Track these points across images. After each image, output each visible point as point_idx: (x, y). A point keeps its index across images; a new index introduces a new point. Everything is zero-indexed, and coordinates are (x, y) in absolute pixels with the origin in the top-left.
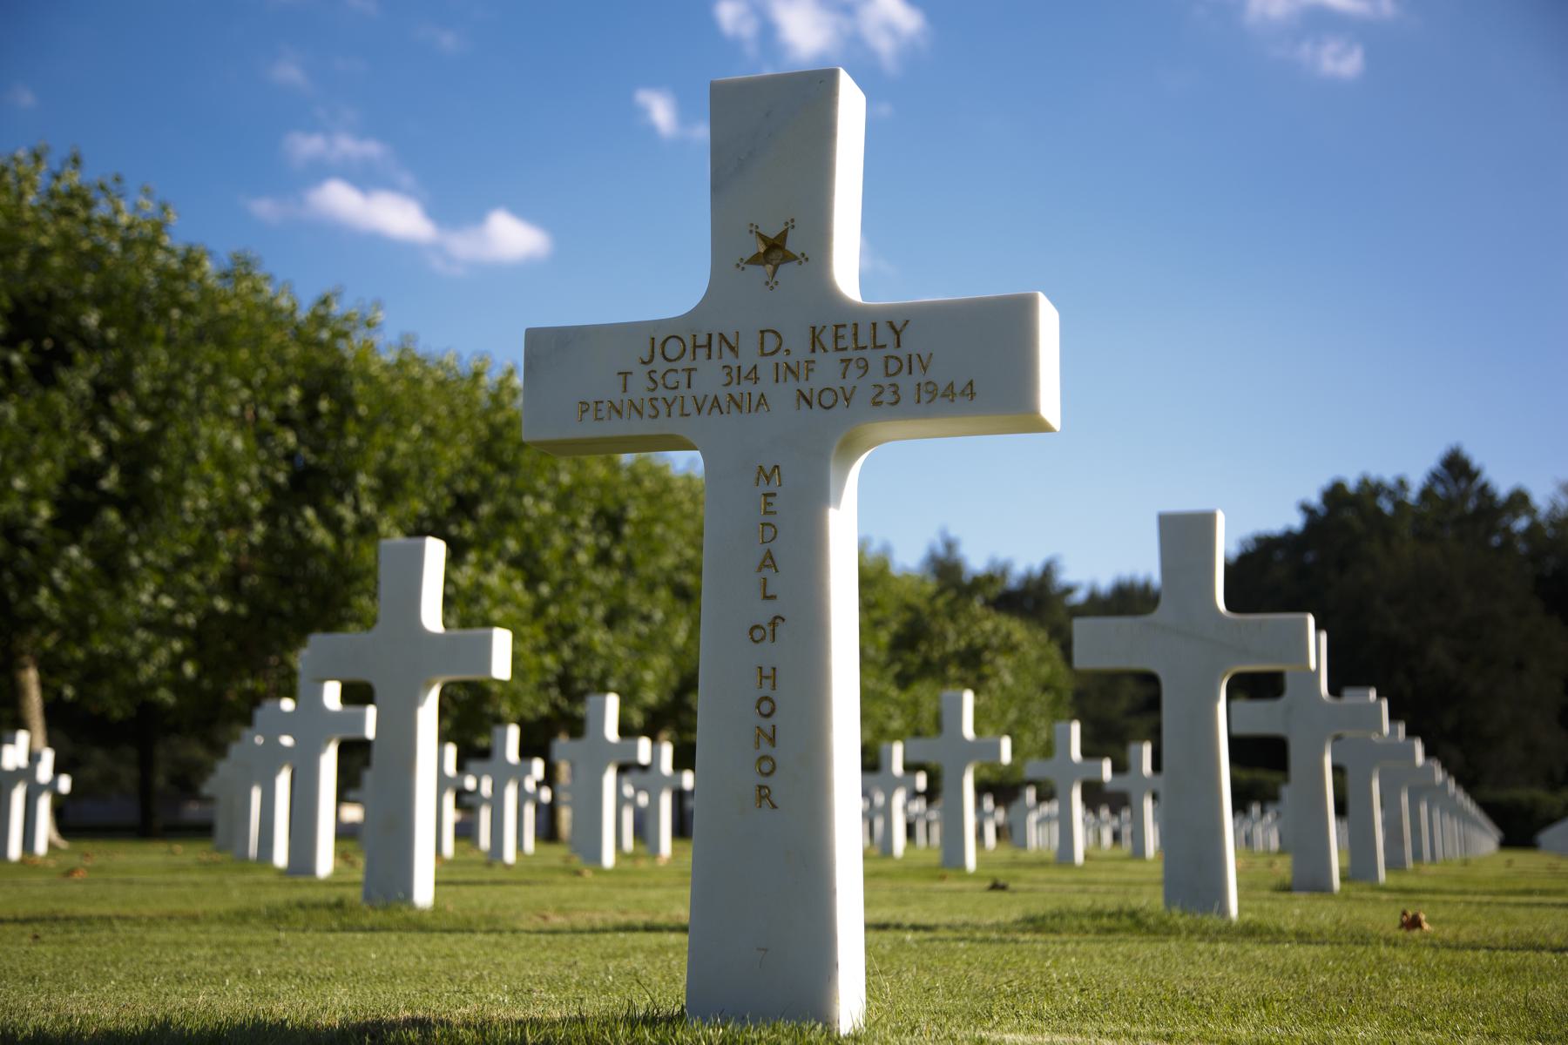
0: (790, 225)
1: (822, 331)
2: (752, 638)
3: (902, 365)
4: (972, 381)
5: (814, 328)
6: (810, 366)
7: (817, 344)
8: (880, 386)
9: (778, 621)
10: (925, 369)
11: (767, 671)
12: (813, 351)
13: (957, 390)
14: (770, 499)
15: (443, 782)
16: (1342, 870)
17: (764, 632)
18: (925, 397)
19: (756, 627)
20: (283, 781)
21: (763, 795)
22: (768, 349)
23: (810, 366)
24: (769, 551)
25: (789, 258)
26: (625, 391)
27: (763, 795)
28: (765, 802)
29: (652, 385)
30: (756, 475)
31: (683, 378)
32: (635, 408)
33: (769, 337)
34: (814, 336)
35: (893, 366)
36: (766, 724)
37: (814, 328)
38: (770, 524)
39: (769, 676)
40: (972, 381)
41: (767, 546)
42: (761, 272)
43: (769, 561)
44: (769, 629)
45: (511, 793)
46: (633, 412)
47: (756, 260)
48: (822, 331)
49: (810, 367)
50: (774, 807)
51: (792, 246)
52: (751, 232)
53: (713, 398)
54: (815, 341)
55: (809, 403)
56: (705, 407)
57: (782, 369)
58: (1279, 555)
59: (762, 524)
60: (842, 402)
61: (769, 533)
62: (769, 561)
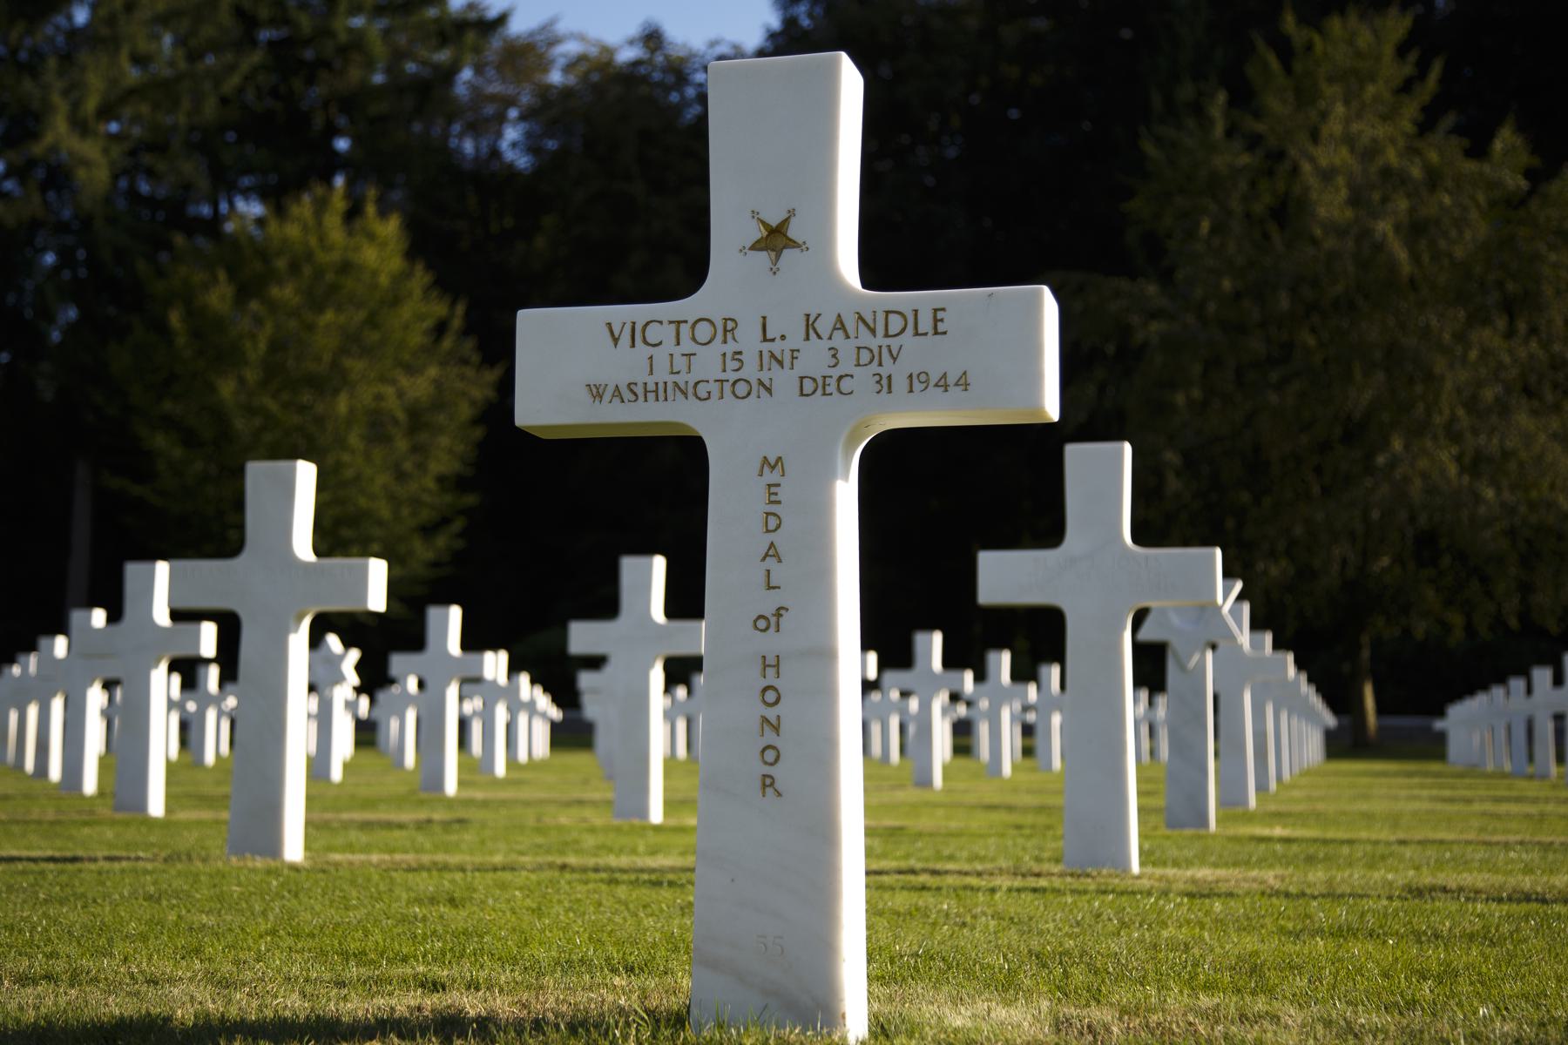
0: (792, 213)
1: (817, 318)
2: (761, 630)
3: (873, 357)
5: (808, 316)
6: (795, 354)
7: (811, 331)
8: (878, 374)
9: (782, 612)
10: (895, 359)
11: (771, 660)
12: (807, 338)
13: (951, 380)
14: (773, 490)
15: (171, 705)
16: (670, 761)
17: (768, 622)
18: (917, 386)
19: (761, 617)
20: (57, 705)
21: (768, 783)
22: (893, 330)
23: (795, 354)
25: (793, 244)
26: (651, 373)
27: (768, 783)
28: (769, 791)
30: (758, 466)
32: (680, 388)
34: (807, 325)
35: (865, 357)
36: (771, 714)
37: (808, 316)
38: (774, 514)
42: (763, 257)
43: (772, 552)
44: (773, 620)
45: (211, 715)
46: (678, 393)
48: (817, 318)
49: (795, 356)
50: (779, 794)
51: (793, 232)
52: (753, 217)
53: (613, 388)
54: (810, 325)
55: (685, 394)
56: (606, 393)
57: (766, 356)
59: (766, 513)
60: (963, 387)
61: (773, 523)
62: (772, 552)
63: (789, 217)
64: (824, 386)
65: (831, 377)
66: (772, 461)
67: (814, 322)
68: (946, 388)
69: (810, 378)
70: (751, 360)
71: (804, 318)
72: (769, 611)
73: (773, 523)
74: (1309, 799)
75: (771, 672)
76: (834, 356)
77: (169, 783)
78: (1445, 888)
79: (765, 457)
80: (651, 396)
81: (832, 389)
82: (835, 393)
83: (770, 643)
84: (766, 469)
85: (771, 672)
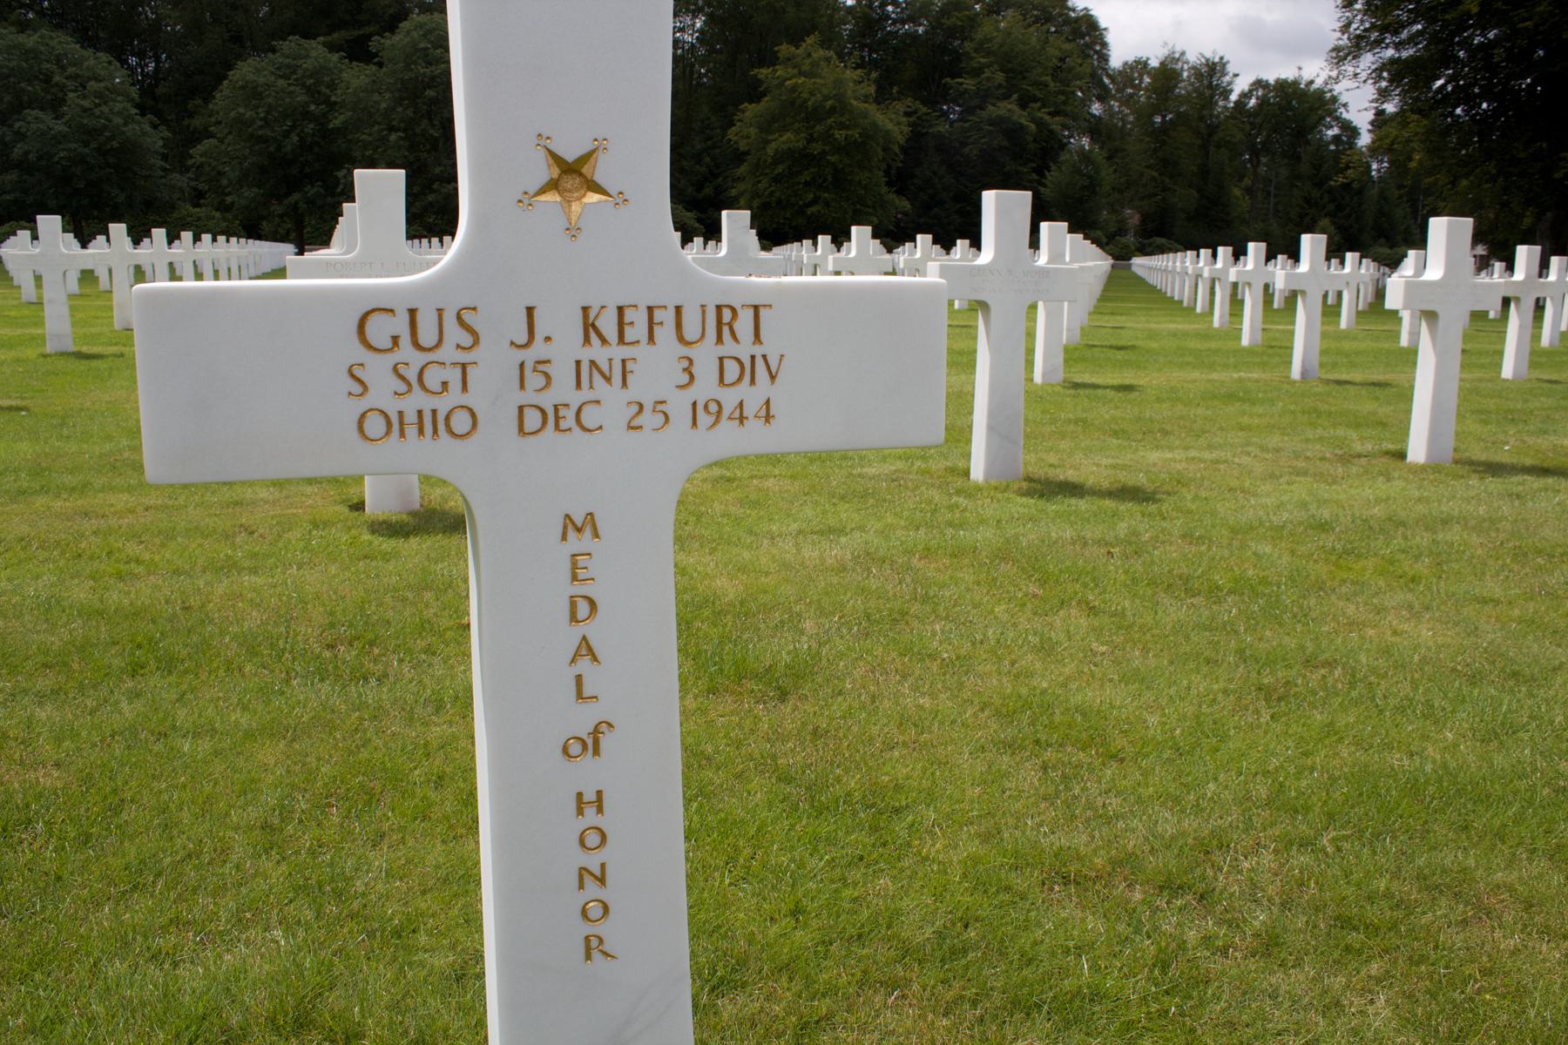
4: (773, 382)
10: (773, 377)
11: (590, 796)
21: (592, 947)
24: (584, 638)
29: (402, 387)
31: (454, 376)
33: (728, 363)
36: (593, 862)
39: (590, 803)
40: (773, 382)
41: (580, 630)
47: (552, 185)
58: (971, 389)
62: (586, 649)
63: (594, 151)
64: (557, 419)
65: (567, 405)
66: (579, 521)
67: (596, 317)
68: (742, 419)
69: (377, 410)
70: (563, 373)
71: (580, 313)
72: (584, 731)
73: (583, 609)
74: (1280, 381)
75: (590, 812)
76: (688, 370)
77: (476, 820)
78: (1186, 579)
79: (567, 516)
80: (411, 431)
81: (569, 421)
82: (576, 429)
83: (588, 774)
84: (571, 533)
85: (590, 812)
